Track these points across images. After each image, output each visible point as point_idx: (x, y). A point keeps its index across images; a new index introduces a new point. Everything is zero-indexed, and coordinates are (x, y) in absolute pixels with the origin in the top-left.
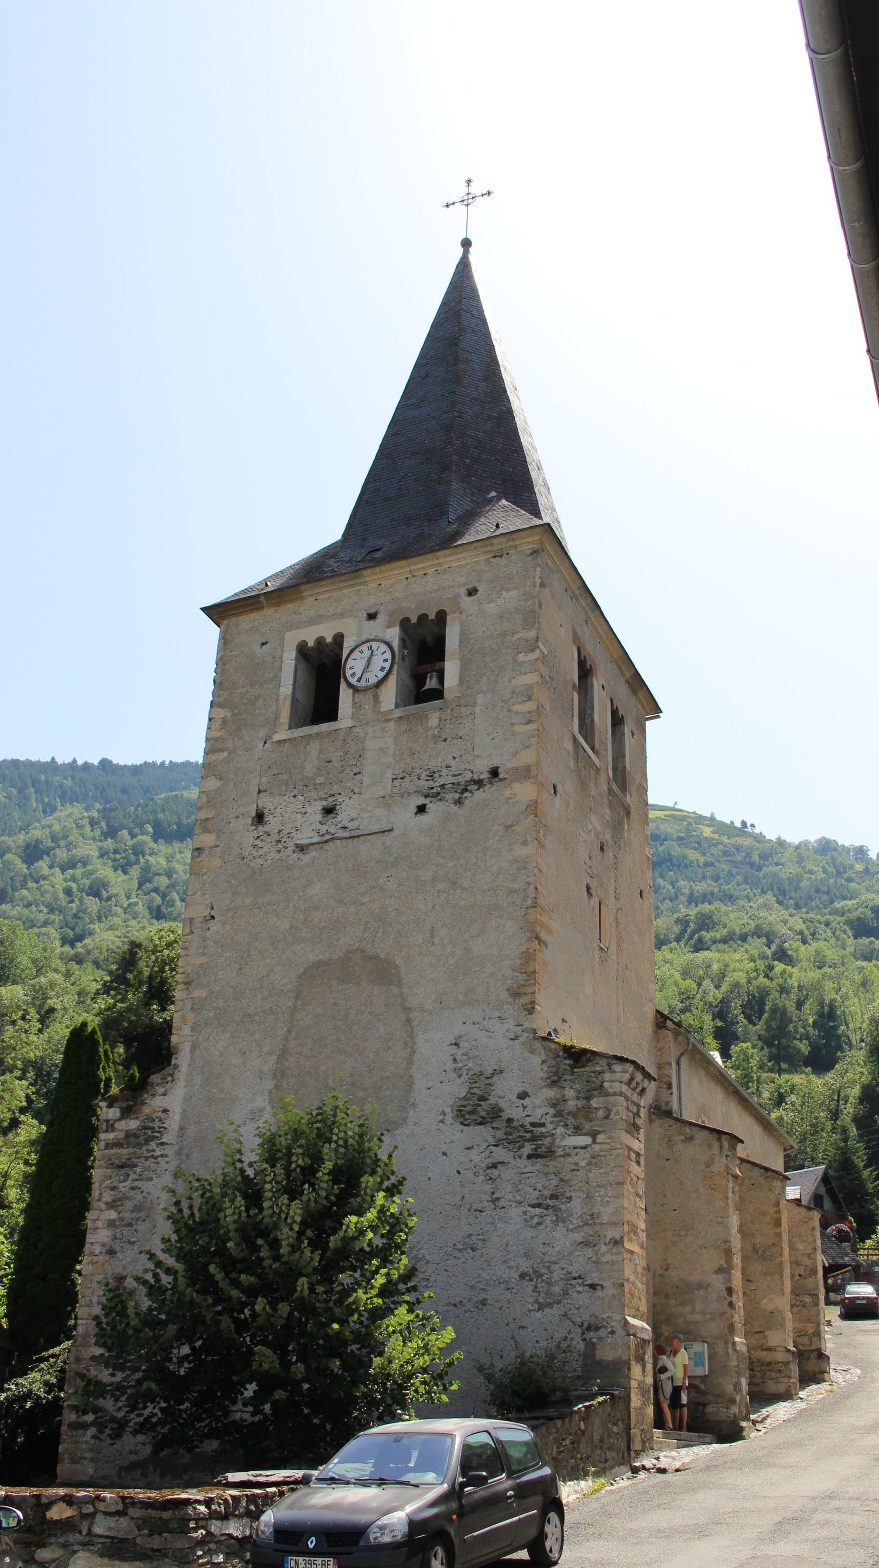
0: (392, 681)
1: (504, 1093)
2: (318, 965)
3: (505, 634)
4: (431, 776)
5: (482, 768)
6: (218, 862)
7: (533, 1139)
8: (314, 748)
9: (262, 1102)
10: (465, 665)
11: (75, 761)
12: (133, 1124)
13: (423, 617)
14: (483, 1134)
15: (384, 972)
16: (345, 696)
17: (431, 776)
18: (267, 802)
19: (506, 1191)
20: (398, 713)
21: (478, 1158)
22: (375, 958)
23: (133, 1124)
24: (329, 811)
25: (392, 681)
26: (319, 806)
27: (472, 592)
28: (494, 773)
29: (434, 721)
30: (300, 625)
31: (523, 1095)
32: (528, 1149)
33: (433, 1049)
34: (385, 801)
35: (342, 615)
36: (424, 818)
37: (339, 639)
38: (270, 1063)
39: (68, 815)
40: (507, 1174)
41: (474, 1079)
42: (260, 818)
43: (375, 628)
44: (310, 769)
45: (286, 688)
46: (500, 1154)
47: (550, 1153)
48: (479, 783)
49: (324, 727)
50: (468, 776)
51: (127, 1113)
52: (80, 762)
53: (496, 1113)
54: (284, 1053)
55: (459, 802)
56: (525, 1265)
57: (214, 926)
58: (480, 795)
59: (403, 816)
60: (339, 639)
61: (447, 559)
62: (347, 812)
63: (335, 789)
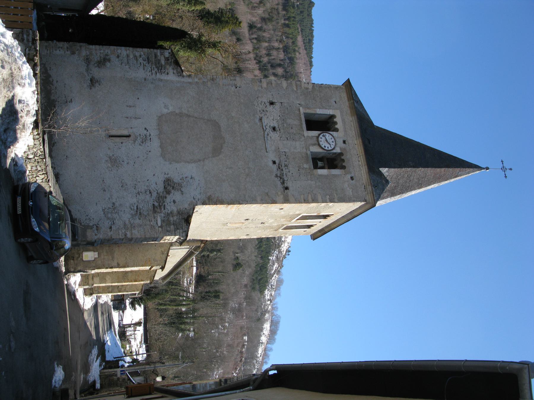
0: (320, 150)
1: (176, 195)
2: (219, 127)
4: (286, 166)
5: (289, 184)
6: (256, 88)
7: (160, 206)
8: (297, 122)
9: (171, 109)
10: (326, 177)
12: (163, 62)
13: (343, 161)
14: (160, 188)
15: (217, 151)
16: (315, 133)
17: (286, 166)
18: (277, 106)
20: (309, 153)
22: (222, 148)
23: (163, 62)
24: (274, 129)
25: (320, 150)
26: (276, 125)
27: (352, 178)
28: (287, 188)
29: (305, 166)
30: (342, 115)
31: (174, 202)
32: (156, 204)
34: (277, 150)
35: (345, 131)
36: (271, 164)
37: (337, 130)
38: (185, 111)
40: (148, 197)
41: (180, 185)
42: (272, 103)
44: (289, 121)
45: (319, 111)
46: (155, 195)
47: (155, 212)
48: (283, 183)
50: (286, 179)
51: (167, 59)
53: (169, 193)
54: (188, 116)
55: (277, 176)
56: (117, 204)
57: (233, 88)
58: (279, 183)
59: (272, 156)
60: (337, 130)
62: (274, 136)
63: (282, 131)
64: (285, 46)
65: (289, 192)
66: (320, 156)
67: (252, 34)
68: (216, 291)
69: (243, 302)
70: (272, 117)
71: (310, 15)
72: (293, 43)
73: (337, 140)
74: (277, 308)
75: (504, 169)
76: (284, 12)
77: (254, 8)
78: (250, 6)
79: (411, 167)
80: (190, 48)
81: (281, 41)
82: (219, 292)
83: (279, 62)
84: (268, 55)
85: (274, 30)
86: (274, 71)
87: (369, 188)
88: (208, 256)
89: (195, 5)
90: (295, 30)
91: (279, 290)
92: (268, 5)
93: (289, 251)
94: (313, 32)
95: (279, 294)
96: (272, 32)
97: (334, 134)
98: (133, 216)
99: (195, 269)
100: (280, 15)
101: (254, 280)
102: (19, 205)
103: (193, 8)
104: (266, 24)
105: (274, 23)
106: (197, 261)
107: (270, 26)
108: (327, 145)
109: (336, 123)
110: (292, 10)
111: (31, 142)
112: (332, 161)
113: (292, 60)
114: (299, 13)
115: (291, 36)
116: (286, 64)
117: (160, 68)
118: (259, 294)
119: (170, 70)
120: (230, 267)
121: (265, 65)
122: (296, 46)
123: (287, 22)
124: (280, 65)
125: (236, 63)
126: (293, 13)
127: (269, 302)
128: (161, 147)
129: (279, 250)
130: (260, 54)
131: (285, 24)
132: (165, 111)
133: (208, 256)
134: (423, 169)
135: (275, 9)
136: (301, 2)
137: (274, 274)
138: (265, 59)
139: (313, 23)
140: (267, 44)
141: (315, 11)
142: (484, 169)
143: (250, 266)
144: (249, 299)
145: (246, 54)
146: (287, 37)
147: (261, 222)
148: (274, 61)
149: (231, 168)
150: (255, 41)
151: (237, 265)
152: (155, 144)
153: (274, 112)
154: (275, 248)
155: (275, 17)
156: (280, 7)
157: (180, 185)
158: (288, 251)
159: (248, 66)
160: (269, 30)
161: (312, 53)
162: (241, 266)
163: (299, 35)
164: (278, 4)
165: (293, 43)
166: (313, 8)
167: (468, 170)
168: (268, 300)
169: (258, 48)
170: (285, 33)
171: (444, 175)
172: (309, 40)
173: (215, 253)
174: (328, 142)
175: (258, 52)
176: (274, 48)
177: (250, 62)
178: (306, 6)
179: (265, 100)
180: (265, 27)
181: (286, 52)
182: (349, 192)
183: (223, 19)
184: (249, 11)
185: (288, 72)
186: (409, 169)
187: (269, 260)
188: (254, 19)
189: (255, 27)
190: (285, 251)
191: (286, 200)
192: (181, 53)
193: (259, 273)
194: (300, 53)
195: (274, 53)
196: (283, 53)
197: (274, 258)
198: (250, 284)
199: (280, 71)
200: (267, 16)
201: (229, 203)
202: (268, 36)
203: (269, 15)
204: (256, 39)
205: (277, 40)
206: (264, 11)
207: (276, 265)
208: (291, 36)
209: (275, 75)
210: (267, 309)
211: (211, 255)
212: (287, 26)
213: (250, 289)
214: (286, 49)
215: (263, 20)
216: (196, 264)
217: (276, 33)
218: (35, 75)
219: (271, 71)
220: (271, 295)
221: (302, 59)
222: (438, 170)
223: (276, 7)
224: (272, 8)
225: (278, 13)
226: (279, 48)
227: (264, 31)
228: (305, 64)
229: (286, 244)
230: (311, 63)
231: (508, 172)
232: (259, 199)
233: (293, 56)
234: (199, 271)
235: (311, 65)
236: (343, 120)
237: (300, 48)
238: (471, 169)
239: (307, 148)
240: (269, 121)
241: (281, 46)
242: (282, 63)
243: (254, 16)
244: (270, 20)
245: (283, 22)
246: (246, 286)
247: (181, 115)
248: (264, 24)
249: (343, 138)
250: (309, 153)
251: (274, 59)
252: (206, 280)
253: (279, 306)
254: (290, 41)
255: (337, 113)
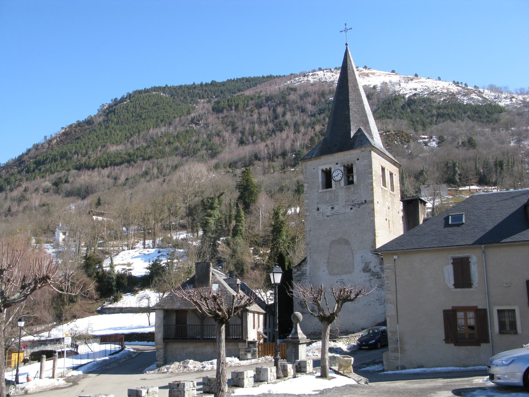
0: (343, 179)
1: (371, 266)
2: (334, 241)
3: (365, 170)
4: (353, 202)
5: (363, 200)
6: (310, 219)
7: (377, 275)
8: (328, 194)
9: (325, 268)
10: (358, 176)
11: (202, 82)
12: (300, 272)
13: (348, 165)
14: (368, 274)
15: (347, 242)
16: (333, 183)
17: (353, 202)
18: (319, 206)
19: (373, 284)
20: (345, 187)
21: (367, 278)
22: (345, 240)
23: (300, 272)
24: (332, 208)
25: (343, 179)
26: (330, 207)
27: (358, 159)
28: (366, 201)
29: (352, 189)
30: (321, 165)
31: (375, 267)
32: (376, 277)
33: (357, 258)
34: (344, 207)
35: (330, 163)
36: (352, 211)
37: (330, 169)
38: (326, 261)
39: (202, 107)
40: (373, 281)
41: (366, 263)
42: (318, 209)
43: (338, 167)
44: (327, 199)
45: (320, 180)
46: (371, 278)
47: (380, 278)
48: (363, 203)
49: (330, 189)
50: (360, 202)
51: (298, 270)
52: (204, 83)
53: (370, 270)
54: (329, 258)
55: (359, 207)
56: (377, 298)
57: (311, 232)
58: (363, 206)
59: (348, 210)
60: (330, 169)
61: (352, 152)
62: (336, 208)
63: (333, 203)
64: (256, 106)
65: (368, 200)
66: (346, 178)
67: (248, 140)
68: (494, 165)
69: (512, 130)
70: (326, 209)
71: (223, 84)
72: (252, 99)
73: (336, 169)
74: (521, 89)
75: (346, 30)
76: (225, 111)
77: (224, 141)
78: (223, 145)
79: (349, 113)
80: (280, 231)
81: (252, 111)
82: (496, 162)
83: (271, 112)
84: (266, 123)
85: (242, 119)
86: (281, 116)
87: (363, 149)
88: (460, 175)
89: (241, 217)
90: (239, 98)
91: (501, 88)
92: (220, 127)
93: (458, 83)
94: (239, 79)
95: (506, 88)
96: (244, 121)
97: (332, 170)
98: (383, 290)
99: (472, 187)
100: (228, 114)
101: (488, 121)
102: (365, 347)
103: (243, 218)
104: (238, 128)
105: (236, 120)
106: (465, 186)
107: (239, 124)
108: (340, 175)
109: (326, 169)
110: (222, 104)
111: (342, 343)
112: (349, 170)
113: (268, 99)
114: (223, 95)
115: (246, 102)
116: (272, 104)
117: (303, 274)
118: (503, 114)
119: (304, 268)
120: (471, 153)
121: (276, 125)
122: (255, 96)
123: (233, 107)
124: (274, 111)
125: (277, 157)
126: (224, 102)
127: (514, 100)
128: (346, 274)
129: (457, 94)
130: (266, 132)
131: (236, 109)
132: (326, 271)
133: (460, 175)
134: (350, 103)
135: (222, 121)
136: (213, 94)
137: (482, 97)
138: (271, 126)
139: (231, 80)
140: (256, 126)
141: (220, 79)
142: (347, 48)
143: (473, 127)
144: (507, 125)
145: (269, 149)
146: (248, 106)
147: (388, 210)
148: (271, 117)
149: (356, 234)
150: (255, 137)
151: (471, 143)
152: (345, 277)
153: (323, 208)
154: (455, 98)
155: (230, 119)
156: (221, 115)
157: (366, 263)
158: (457, 84)
159: (279, 145)
160: (243, 124)
161: (258, 78)
162: (471, 138)
163: (244, 94)
164: (218, 118)
165: (252, 99)
166: (217, 81)
167: (348, 62)
168: (511, 100)
169: (260, 133)
170: (244, 107)
171: (353, 83)
172: (246, 82)
173: (457, 168)
174: (338, 175)
175: (264, 134)
176: (259, 118)
177: (275, 144)
178: (217, 88)
179: (316, 213)
180: (240, 129)
181: (261, 105)
182: (366, 162)
183: (245, 184)
184: (227, 146)
185: (280, 101)
186: (351, 114)
187: (467, 104)
188: (235, 140)
189: (241, 138)
190: (457, 88)
191: (372, 202)
192: (284, 237)
193: (481, 115)
194: (261, 91)
195: (263, 117)
196: (262, 109)
197: (465, 98)
198: (491, 124)
199: (280, 110)
200: (230, 127)
201: (375, 236)
202: (248, 124)
203: (229, 125)
204: (252, 137)
205: (252, 116)
206: (226, 131)
207: (473, 96)
208: (246, 102)
209: (284, 115)
210: (521, 101)
211: (459, 172)
212: (237, 107)
213: (496, 125)
214: (259, 106)
215: (234, 130)
216: (468, 185)
217: (245, 116)
218: (316, 342)
219: (281, 119)
220: (505, 98)
221: (266, 89)
222: (350, 89)
223: (221, 119)
224: (222, 123)
225: (226, 116)
226: (259, 113)
227: (244, 129)
228: (270, 85)
229: (450, 87)
230: (268, 77)
231: (348, 27)
232: (372, 218)
233: (264, 98)
234: (474, 184)
235: (270, 77)
236: (324, 164)
237: (256, 92)
238: (348, 59)
239: (342, 188)
240: (329, 212)
241: (256, 111)
242: (272, 108)
243: (232, 141)
244: (233, 124)
245: (233, 111)
246: (493, 129)
247: (328, 263)
248: (238, 130)
249: (335, 162)
250: (345, 187)
251: (269, 117)
252: (484, 175)
253: (518, 87)
254: (251, 102)
255: (321, 168)
